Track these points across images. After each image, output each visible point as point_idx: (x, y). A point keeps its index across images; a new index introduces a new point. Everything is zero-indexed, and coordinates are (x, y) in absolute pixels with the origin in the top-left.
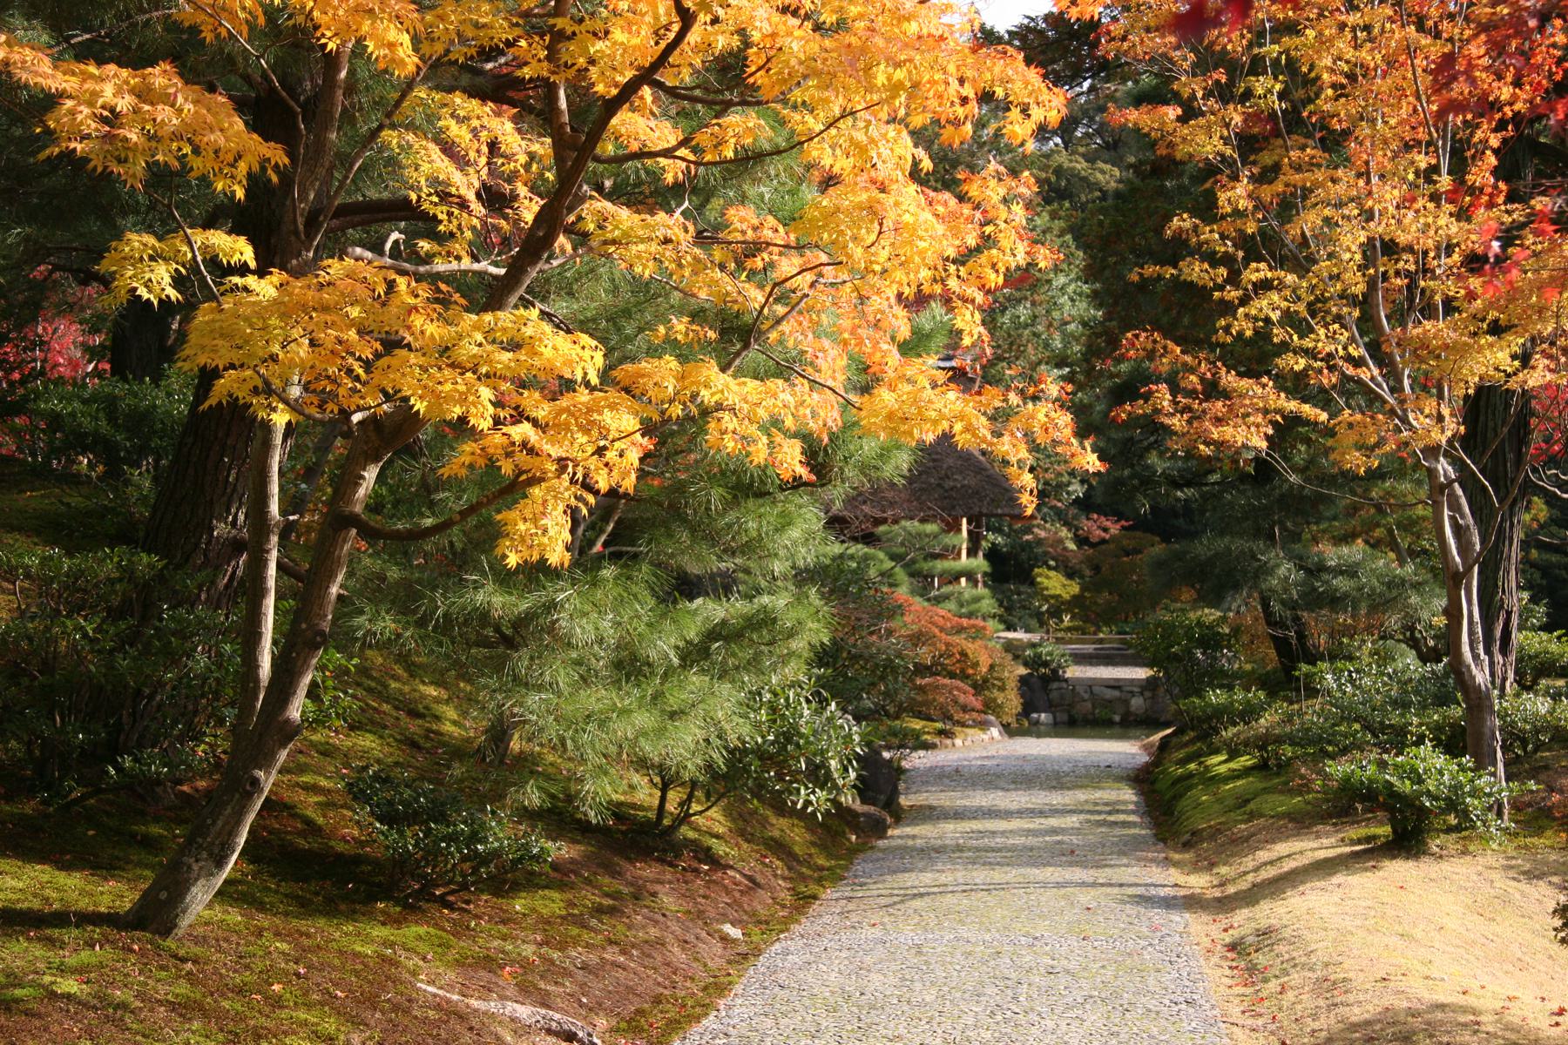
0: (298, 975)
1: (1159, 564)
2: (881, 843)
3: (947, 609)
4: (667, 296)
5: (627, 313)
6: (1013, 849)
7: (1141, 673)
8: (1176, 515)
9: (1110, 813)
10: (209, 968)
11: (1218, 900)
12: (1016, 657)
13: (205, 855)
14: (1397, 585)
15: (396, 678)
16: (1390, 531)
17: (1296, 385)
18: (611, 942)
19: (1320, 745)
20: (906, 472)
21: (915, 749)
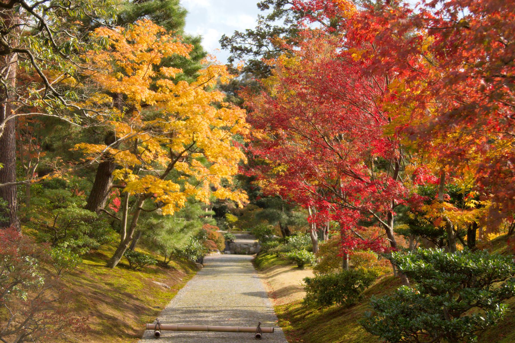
7: (253, 241)
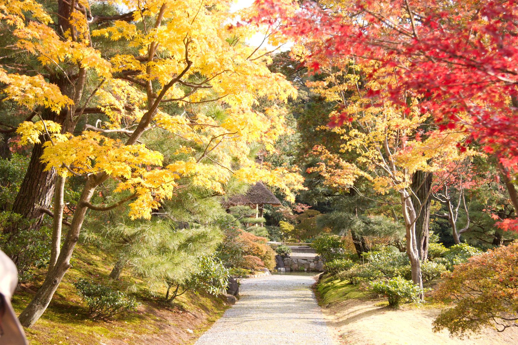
0: (67, 339)
1: (320, 221)
2: (233, 306)
3: (252, 234)
4: (174, 137)
5: (162, 143)
6: (274, 308)
7: (314, 255)
8: (325, 205)
9: (304, 298)
10: (41, 336)
11: (337, 323)
12: (274, 250)
13: (40, 303)
14: (393, 228)
15: (83, 252)
16: (392, 211)
17: (363, 167)
18: (155, 333)
19: (368, 277)
20: (246, 192)
21: (243, 277)
